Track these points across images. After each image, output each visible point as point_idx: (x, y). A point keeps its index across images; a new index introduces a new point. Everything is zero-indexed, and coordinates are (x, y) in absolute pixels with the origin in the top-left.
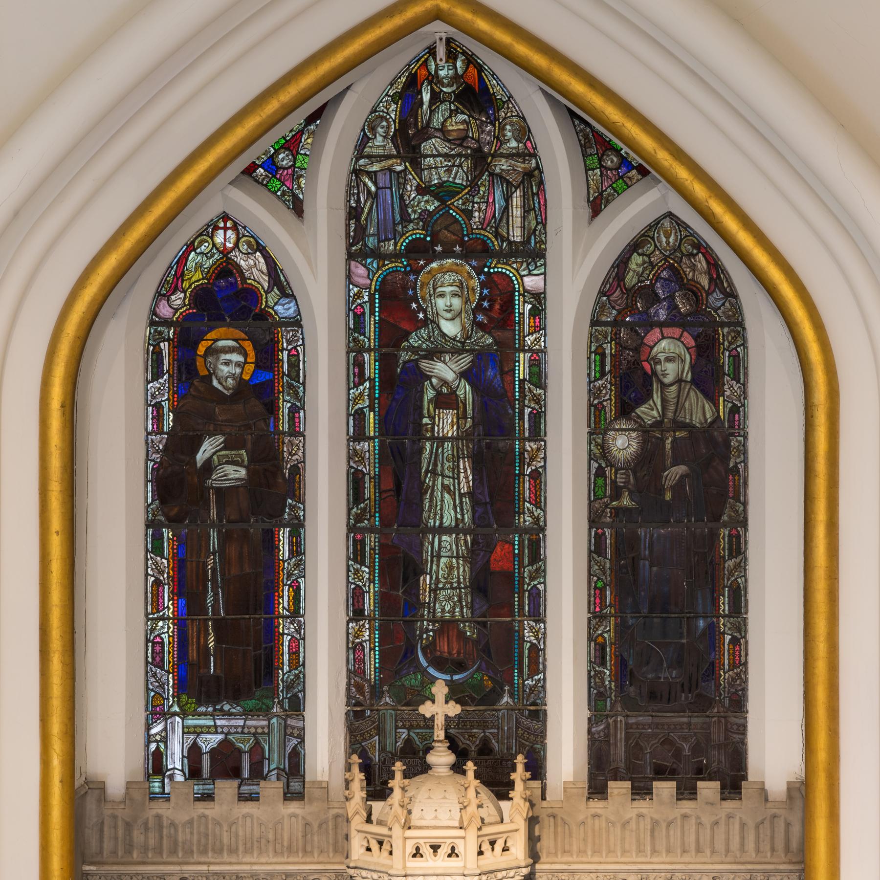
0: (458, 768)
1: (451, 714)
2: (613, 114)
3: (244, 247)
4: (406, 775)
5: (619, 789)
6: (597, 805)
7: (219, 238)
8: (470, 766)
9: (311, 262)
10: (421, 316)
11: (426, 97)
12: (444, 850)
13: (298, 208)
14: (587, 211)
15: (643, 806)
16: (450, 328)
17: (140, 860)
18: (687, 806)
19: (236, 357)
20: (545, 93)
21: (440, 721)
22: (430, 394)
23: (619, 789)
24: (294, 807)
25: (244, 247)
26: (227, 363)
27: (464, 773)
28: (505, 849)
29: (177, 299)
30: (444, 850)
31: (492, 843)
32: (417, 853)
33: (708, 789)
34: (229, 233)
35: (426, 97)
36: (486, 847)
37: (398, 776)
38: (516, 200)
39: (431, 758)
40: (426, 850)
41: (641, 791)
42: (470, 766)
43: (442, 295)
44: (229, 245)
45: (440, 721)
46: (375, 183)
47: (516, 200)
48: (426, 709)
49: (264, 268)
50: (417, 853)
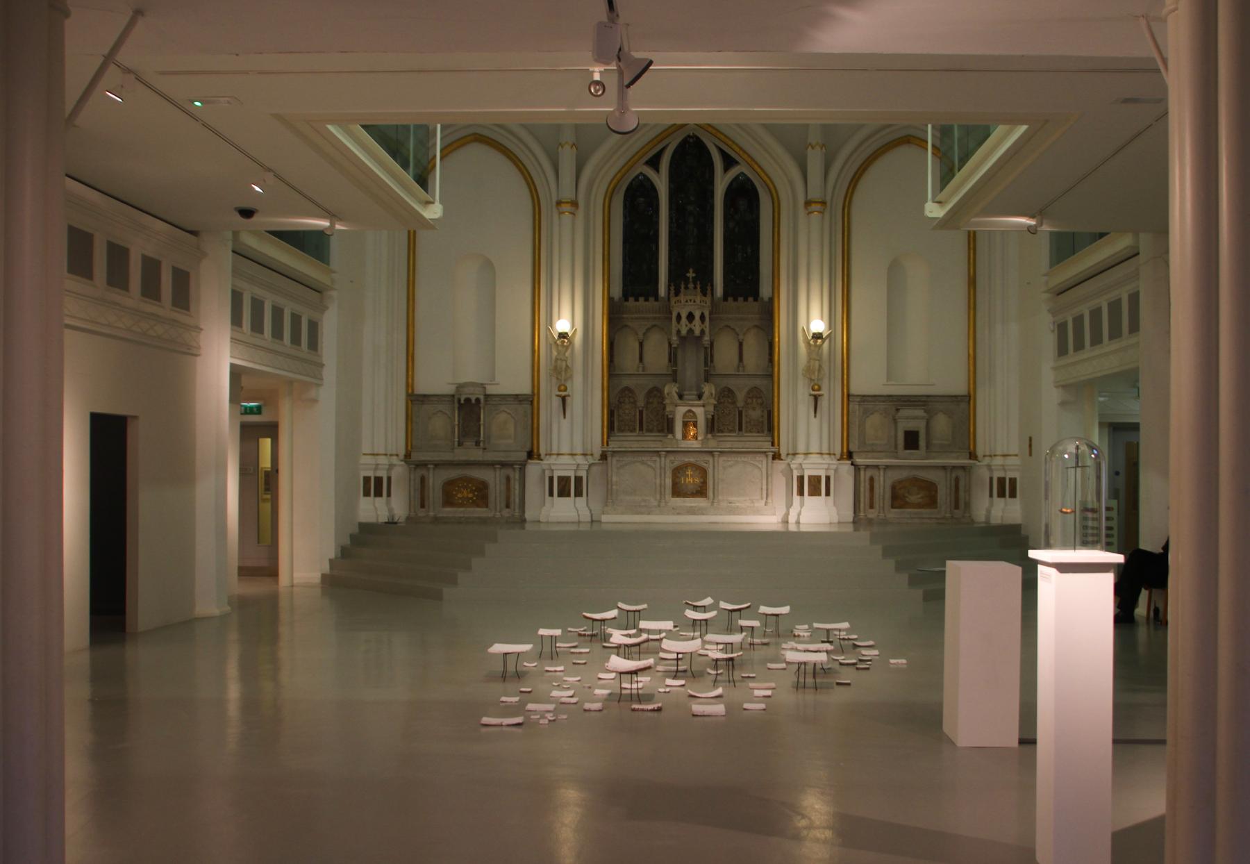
24: (656, 303)
33: (751, 299)
41: (735, 300)
48: (688, 275)
50: (687, 301)
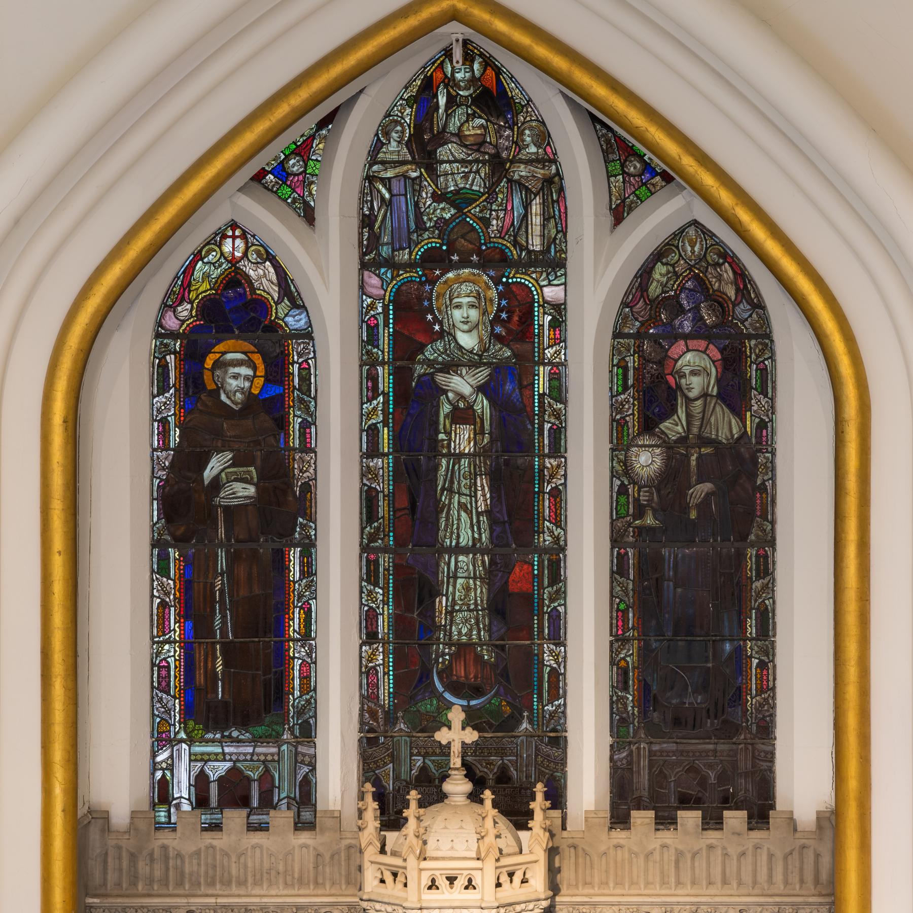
0: (475, 797)
1: (468, 741)
2: (636, 118)
3: (253, 257)
4: (422, 804)
5: (642, 818)
6: (619, 835)
7: (227, 247)
8: (488, 795)
9: (322, 272)
10: (437, 327)
11: (442, 100)
12: (461, 882)
13: (309, 216)
14: (609, 219)
15: (667, 836)
16: (467, 341)
17: (145, 892)
18: (713, 836)
19: (245, 371)
20: (566, 97)
21: (456, 748)
22: (446, 408)
23: (642, 818)
24: (305, 838)
25: (253, 257)
26: (236, 377)
27: (481, 802)
28: (524, 881)
29: (184, 310)
30: (461, 882)
31: (511, 875)
32: (433, 885)
33: (735, 818)
34: (238, 242)
35: (442, 100)
36: (504, 879)
37: (413, 805)
38: (536, 207)
39: (447, 787)
40: (442, 882)
41: (665, 820)
42: (488, 795)
43: (458, 306)
44: (238, 254)
45: (456, 748)
46: (389, 190)
47: (536, 207)
48: (442, 736)
49: (274, 278)
50: (433, 885)
